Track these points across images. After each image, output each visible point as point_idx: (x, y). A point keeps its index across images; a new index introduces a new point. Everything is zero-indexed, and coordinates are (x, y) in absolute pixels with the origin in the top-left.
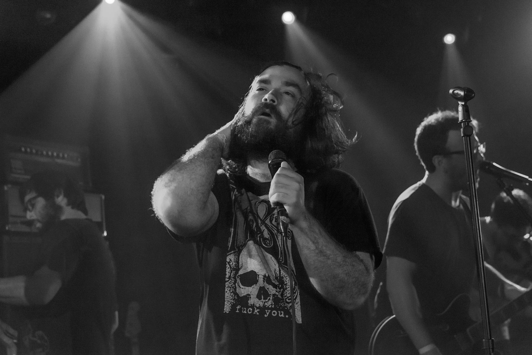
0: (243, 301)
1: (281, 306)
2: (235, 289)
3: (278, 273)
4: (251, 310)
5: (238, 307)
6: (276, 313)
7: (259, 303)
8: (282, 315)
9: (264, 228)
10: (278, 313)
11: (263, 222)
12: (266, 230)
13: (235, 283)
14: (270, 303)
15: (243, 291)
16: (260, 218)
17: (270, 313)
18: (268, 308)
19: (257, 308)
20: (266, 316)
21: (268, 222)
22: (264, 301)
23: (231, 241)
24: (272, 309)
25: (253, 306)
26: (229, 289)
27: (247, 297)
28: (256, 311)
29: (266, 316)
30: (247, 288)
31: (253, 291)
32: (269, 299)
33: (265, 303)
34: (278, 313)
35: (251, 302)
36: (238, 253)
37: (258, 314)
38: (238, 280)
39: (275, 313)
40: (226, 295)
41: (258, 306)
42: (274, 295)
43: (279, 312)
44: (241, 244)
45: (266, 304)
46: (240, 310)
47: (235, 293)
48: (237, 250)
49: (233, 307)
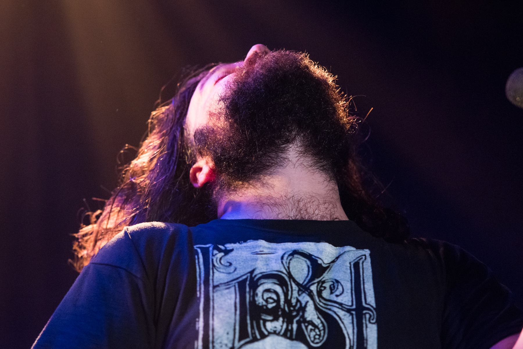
9: (307, 298)
16: (295, 281)
21: (314, 288)
36: (287, 335)
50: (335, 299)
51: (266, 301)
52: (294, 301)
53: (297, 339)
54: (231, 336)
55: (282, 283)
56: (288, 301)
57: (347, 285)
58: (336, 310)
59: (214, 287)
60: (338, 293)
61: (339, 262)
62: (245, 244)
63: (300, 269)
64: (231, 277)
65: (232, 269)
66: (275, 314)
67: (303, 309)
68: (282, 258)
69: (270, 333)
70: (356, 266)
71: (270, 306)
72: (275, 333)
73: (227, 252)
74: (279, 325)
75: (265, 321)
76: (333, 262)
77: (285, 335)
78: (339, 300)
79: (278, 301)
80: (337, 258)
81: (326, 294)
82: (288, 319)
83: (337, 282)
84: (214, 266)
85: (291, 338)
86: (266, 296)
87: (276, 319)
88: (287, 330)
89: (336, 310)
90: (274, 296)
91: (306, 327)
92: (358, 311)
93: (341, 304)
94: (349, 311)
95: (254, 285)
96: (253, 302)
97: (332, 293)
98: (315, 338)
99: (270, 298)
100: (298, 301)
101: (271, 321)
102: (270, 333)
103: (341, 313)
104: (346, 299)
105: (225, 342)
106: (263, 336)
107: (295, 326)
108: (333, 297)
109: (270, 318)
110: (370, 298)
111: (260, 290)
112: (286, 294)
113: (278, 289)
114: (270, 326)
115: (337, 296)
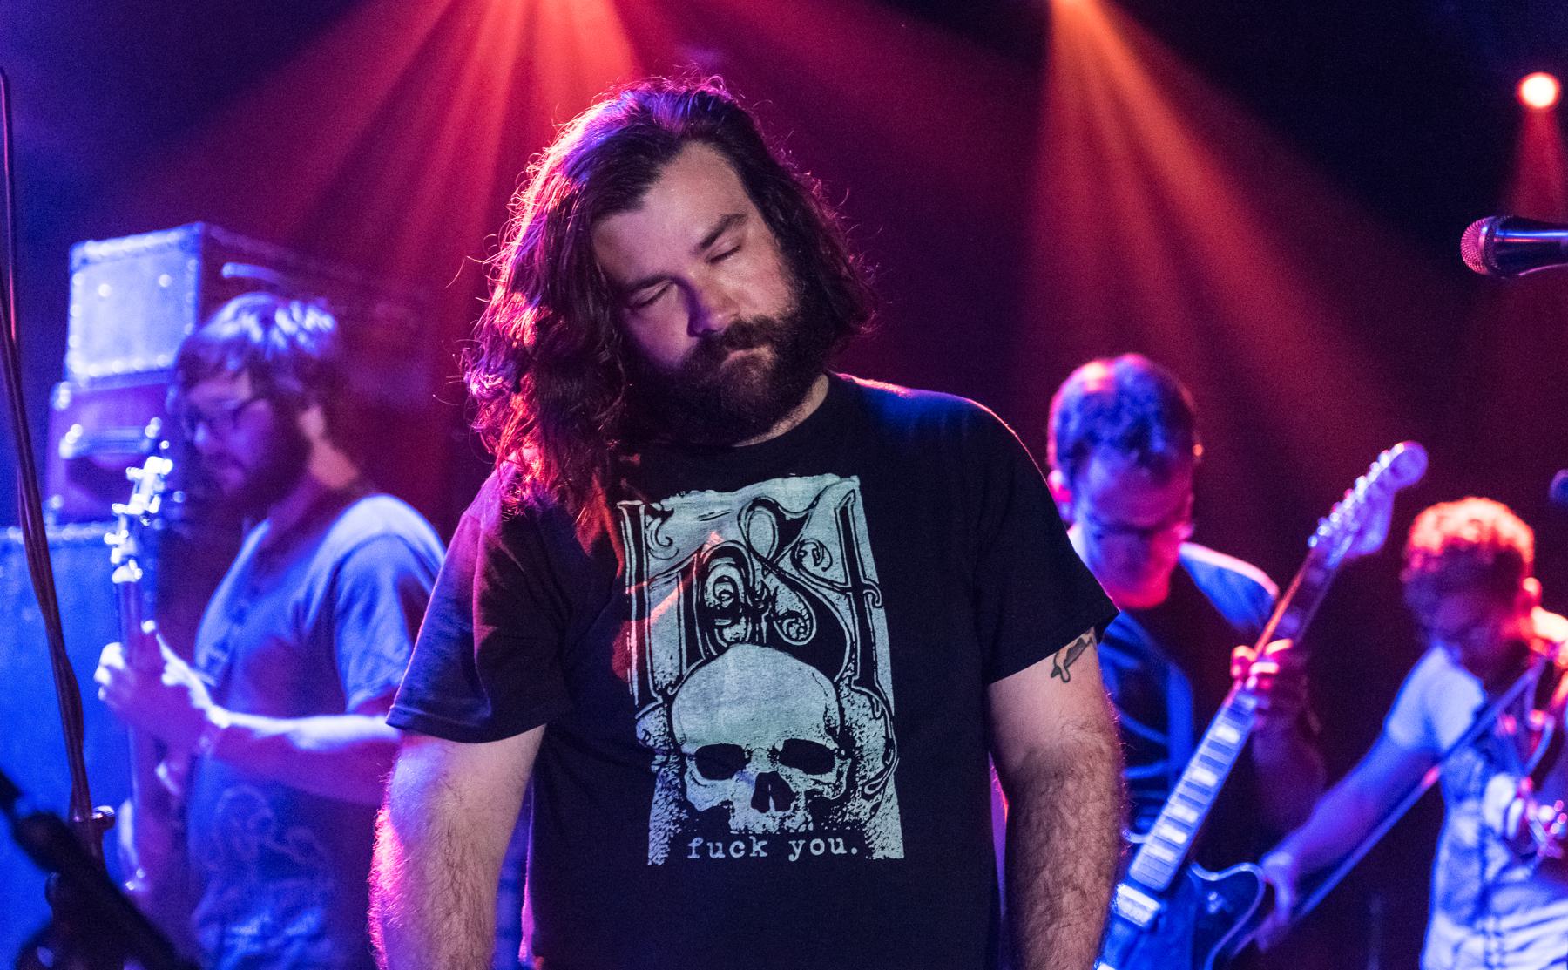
0: (716, 821)
1: (835, 824)
2: (683, 791)
3: (837, 716)
4: (742, 846)
5: (696, 843)
6: (822, 845)
7: (768, 821)
8: (841, 850)
9: (776, 582)
10: (828, 846)
11: (770, 565)
12: (782, 586)
13: (681, 775)
14: (800, 816)
15: (705, 794)
16: (757, 555)
17: (806, 848)
18: (797, 836)
19: (759, 838)
20: (792, 858)
21: (786, 564)
22: (780, 814)
23: (635, 679)
24: (808, 836)
25: (745, 835)
26: (664, 793)
27: (722, 812)
28: (757, 847)
29: (792, 858)
30: (719, 783)
31: (737, 790)
32: (796, 808)
33: (783, 820)
34: (828, 846)
35: (736, 823)
36: (754, 639)
37: (763, 854)
38: (692, 765)
39: (818, 847)
40: (655, 810)
41: (759, 830)
42: (809, 794)
43: (831, 841)
44: (669, 679)
45: (788, 823)
46: (702, 850)
47: (684, 804)
48: (660, 700)
49: (677, 844)
50: (822, 575)
51: (720, 598)
52: (758, 587)
53: (768, 645)
54: (676, 662)
55: (740, 564)
56: (750, 591)
57: (836, 551)
58: (825, 591)
59: (651, 581)
60: (824, 564)
61: (820, 508)
62: (688, 498)
63: (763, 532)
64: (672, 563)
65: (673, 549)
66: (733, 614)
67: (772, 599)
68: (739, 518)
69: (730, 644)
70: (844, 514)
71: (726, 604)
72: (737, 641)
73: (665, 515)
74: (740, 629)
75: (721, 628)
76: (812, 506)
77: (752, 641)
78: (828, 575)
79: (735, 595)
80: (817, 498)
81: (808, 562)
82: (753, 615)
83: (822, 546)
84: (648, 547)
85: (761, 644)
86: (719, 589)
87: (736, 622)
88: (754, 632)
89: (825, 591)
90: (730, 588)
91: (780, 626)
92: (856, 591)
93: (831, 582)
94: (843, 591)
95: (704, 574)
96: (701, 602)
97: (816, 565)
98: (798, 633)
99: (725, 592)
100: (764, 586)
101: (729, 626)
102: (730, 644)
103: (833, 596)
104: (837, 573)
105: (669, 670)
106: (721, 651)
107: (764, 625)
108: (818, 571)
109: (728, 622)
110: (870, 571)
111: (712, 579)
112: (745, 580)
113: (734, 574)
114: (728, 634)
115: (824, 570)
